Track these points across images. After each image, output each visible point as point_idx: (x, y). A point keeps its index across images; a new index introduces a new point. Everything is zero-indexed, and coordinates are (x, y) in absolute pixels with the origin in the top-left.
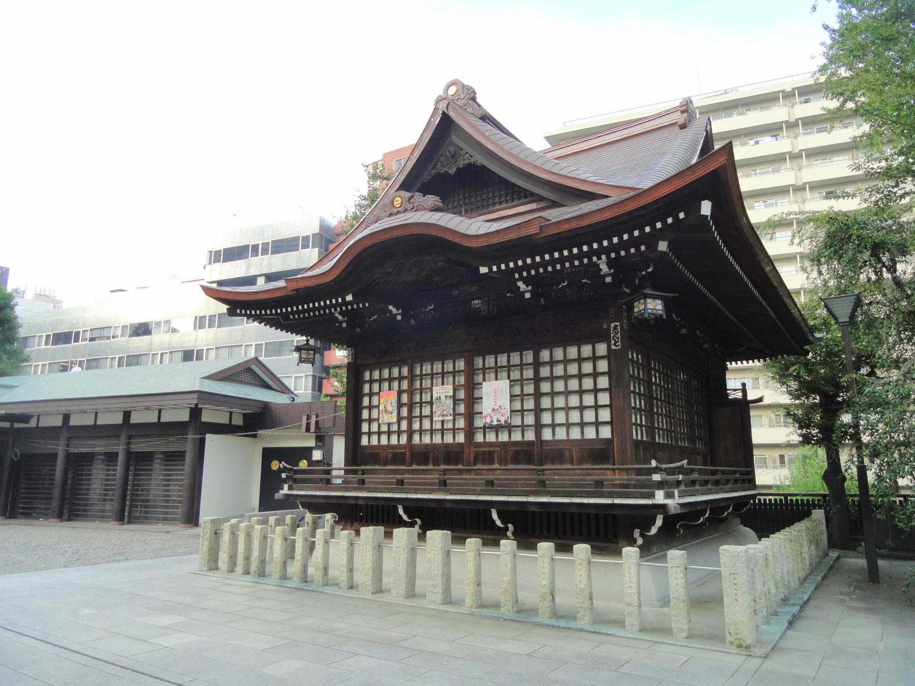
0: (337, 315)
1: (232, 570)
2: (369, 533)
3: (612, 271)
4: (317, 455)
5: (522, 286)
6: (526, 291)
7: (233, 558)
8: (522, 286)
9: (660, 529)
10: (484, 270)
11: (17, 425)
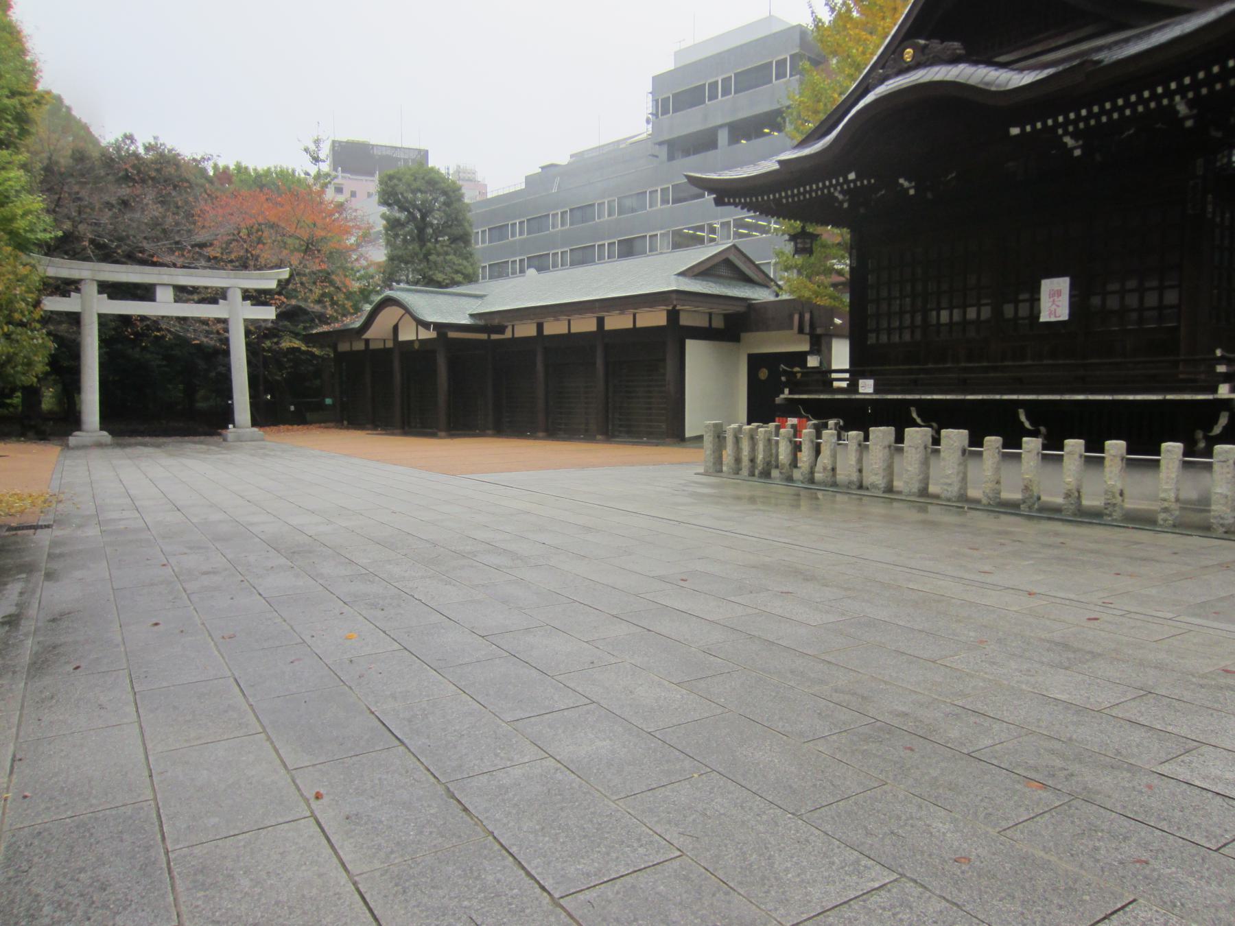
0: (836, 194)
1: (737, 471)
2: (881, 435)
3: (1195, 111)
4: (813, 362)
5: (1068, 140)
6: (1076, 148)
7: (738, 460)
8: (1068, 140)
9: (1225, 428)
10: (1015, 131)
11: (494, 337)
